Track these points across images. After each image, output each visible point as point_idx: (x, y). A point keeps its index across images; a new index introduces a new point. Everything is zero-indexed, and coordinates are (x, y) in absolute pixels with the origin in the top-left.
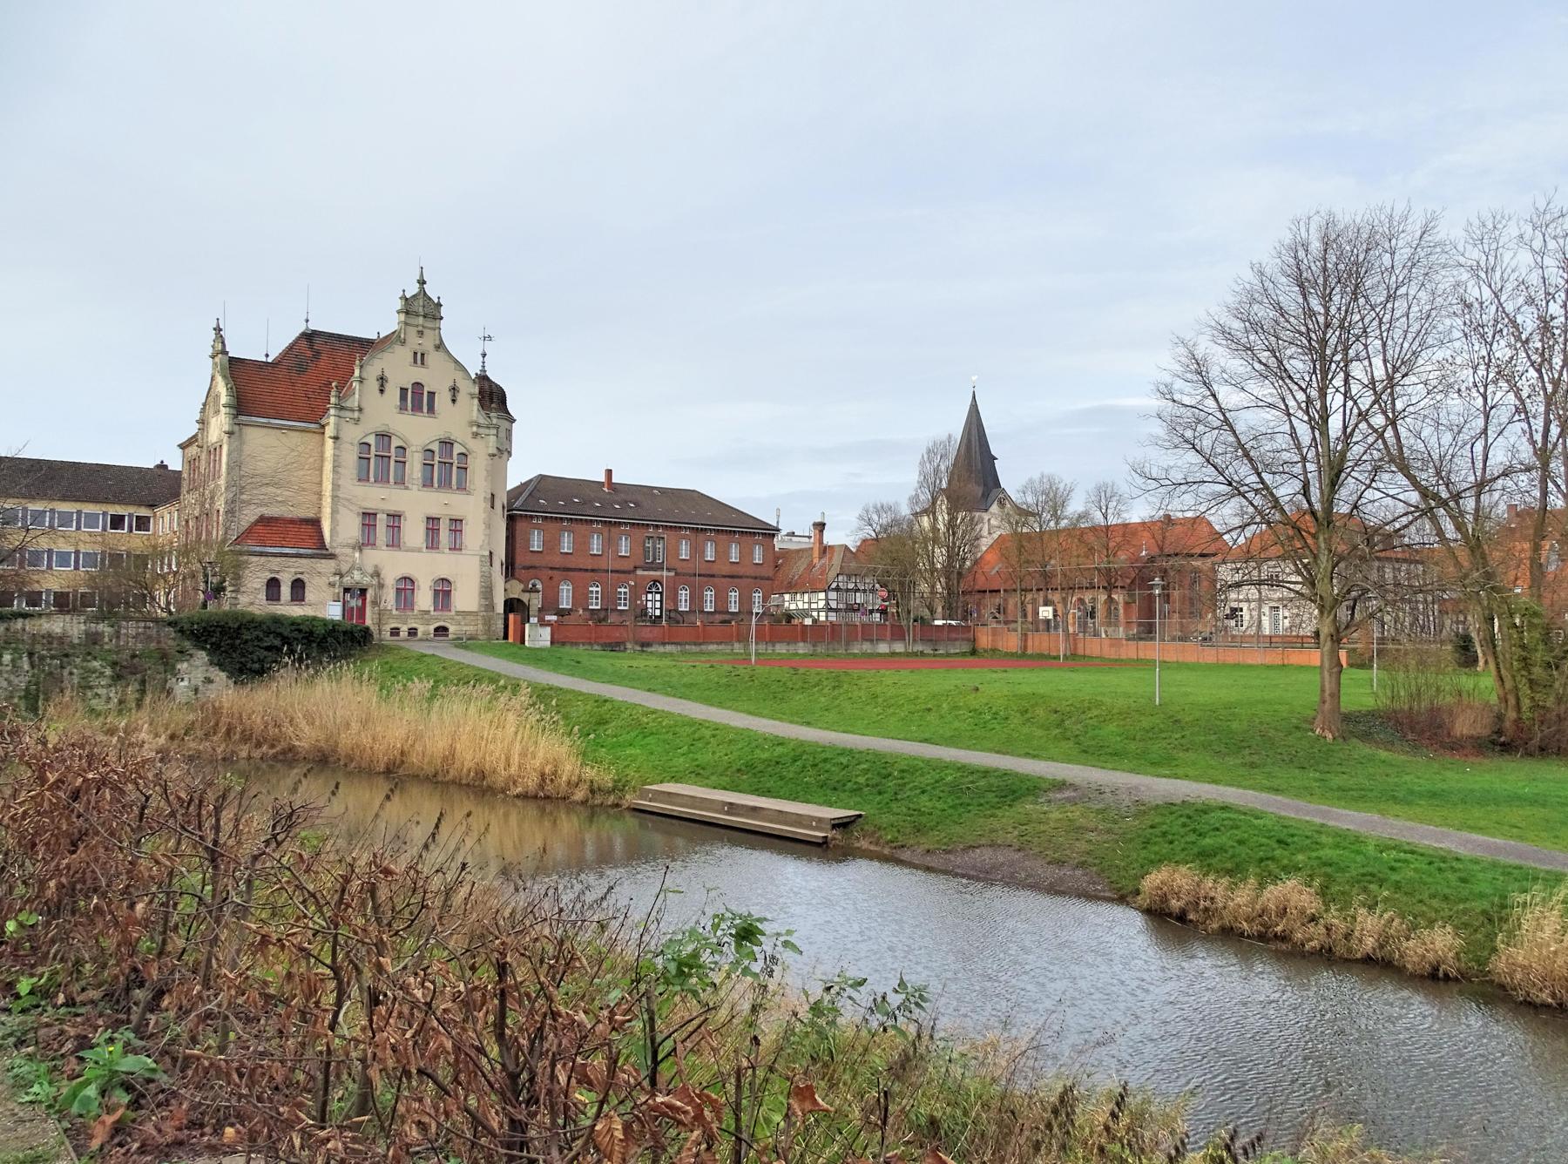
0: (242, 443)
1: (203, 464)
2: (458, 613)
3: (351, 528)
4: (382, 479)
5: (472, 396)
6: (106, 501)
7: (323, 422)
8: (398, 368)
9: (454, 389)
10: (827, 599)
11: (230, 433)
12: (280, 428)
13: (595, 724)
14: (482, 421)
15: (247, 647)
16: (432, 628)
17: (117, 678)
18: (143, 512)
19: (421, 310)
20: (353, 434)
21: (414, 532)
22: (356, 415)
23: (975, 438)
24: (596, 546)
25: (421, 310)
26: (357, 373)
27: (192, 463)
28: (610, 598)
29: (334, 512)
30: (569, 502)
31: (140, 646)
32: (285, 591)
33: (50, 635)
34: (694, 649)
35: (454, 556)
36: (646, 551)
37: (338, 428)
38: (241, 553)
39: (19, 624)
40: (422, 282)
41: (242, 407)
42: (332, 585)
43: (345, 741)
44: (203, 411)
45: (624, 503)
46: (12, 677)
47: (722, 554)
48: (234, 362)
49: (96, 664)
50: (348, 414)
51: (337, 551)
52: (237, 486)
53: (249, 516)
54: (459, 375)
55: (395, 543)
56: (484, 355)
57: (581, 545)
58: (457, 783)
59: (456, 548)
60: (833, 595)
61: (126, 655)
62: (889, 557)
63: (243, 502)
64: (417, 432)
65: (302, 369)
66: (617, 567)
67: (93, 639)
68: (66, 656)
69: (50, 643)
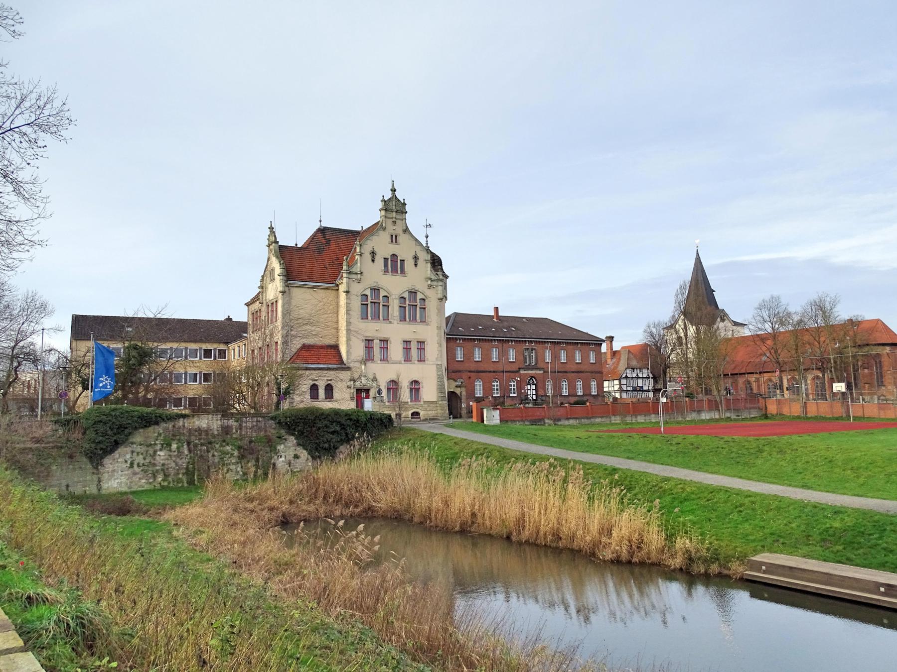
0: (291, 298)
1: (263, 314)
2: (425, 402)
3: (359, 350)
4: (376, 317)
5: (427, 262)
6: (201, 341)
7: (338, 282)
8: (382, 245)
9: (416, 258)
10: (620, 384)
11: (283, 292)
12: (313, 288)
13: (670, 500)
14: (433, 277)
15: (327, 434)
16: (410, 413)
17: (241, 457)
18: (222, 347)
19: (394, 207)
20: (358, 289)
21: (396, 351)
22: (359, 276)
23: (700, 278)
24: (495, 357)
25: (394, 207)
26: (358, 250)
27: (255, 315)
28: (505, 388)
29: (348, 340)
30: (477, 329)
31: (254, 434)
32: (322, 392)
33: (200, 429)
34: (587, 421)
35: (421, 366)
36: (525, 357)
37: (348, 284)
38: (299, 369)
39: (181, 422)
40: (394, 190)
41: (289, 275)
42: (349, 387)
43: (422, 502)
44: (262, 280)
45: (508, 328)
46: (178, 460)
47: (571, 357)
48: (281, 247)
49: (228, 448)
50: (354, 276)
51: (351, 365)
52: (288, 326)
53: (296, 344)
54: (418, 248)
55: (385, 359)
56: (427, 237)
57: (486, 356)
58: (533, 544)
59: (421, 360)
60: (624, 382)
61: (246, 441)
62: (652, 358)
63: (292, 336)
64: (395, 286)
65: (321, 251)
66: (509, 369)
67: (226, 430)
68: (210, 443)
69: (200, 435)
